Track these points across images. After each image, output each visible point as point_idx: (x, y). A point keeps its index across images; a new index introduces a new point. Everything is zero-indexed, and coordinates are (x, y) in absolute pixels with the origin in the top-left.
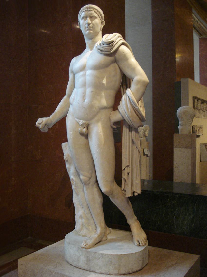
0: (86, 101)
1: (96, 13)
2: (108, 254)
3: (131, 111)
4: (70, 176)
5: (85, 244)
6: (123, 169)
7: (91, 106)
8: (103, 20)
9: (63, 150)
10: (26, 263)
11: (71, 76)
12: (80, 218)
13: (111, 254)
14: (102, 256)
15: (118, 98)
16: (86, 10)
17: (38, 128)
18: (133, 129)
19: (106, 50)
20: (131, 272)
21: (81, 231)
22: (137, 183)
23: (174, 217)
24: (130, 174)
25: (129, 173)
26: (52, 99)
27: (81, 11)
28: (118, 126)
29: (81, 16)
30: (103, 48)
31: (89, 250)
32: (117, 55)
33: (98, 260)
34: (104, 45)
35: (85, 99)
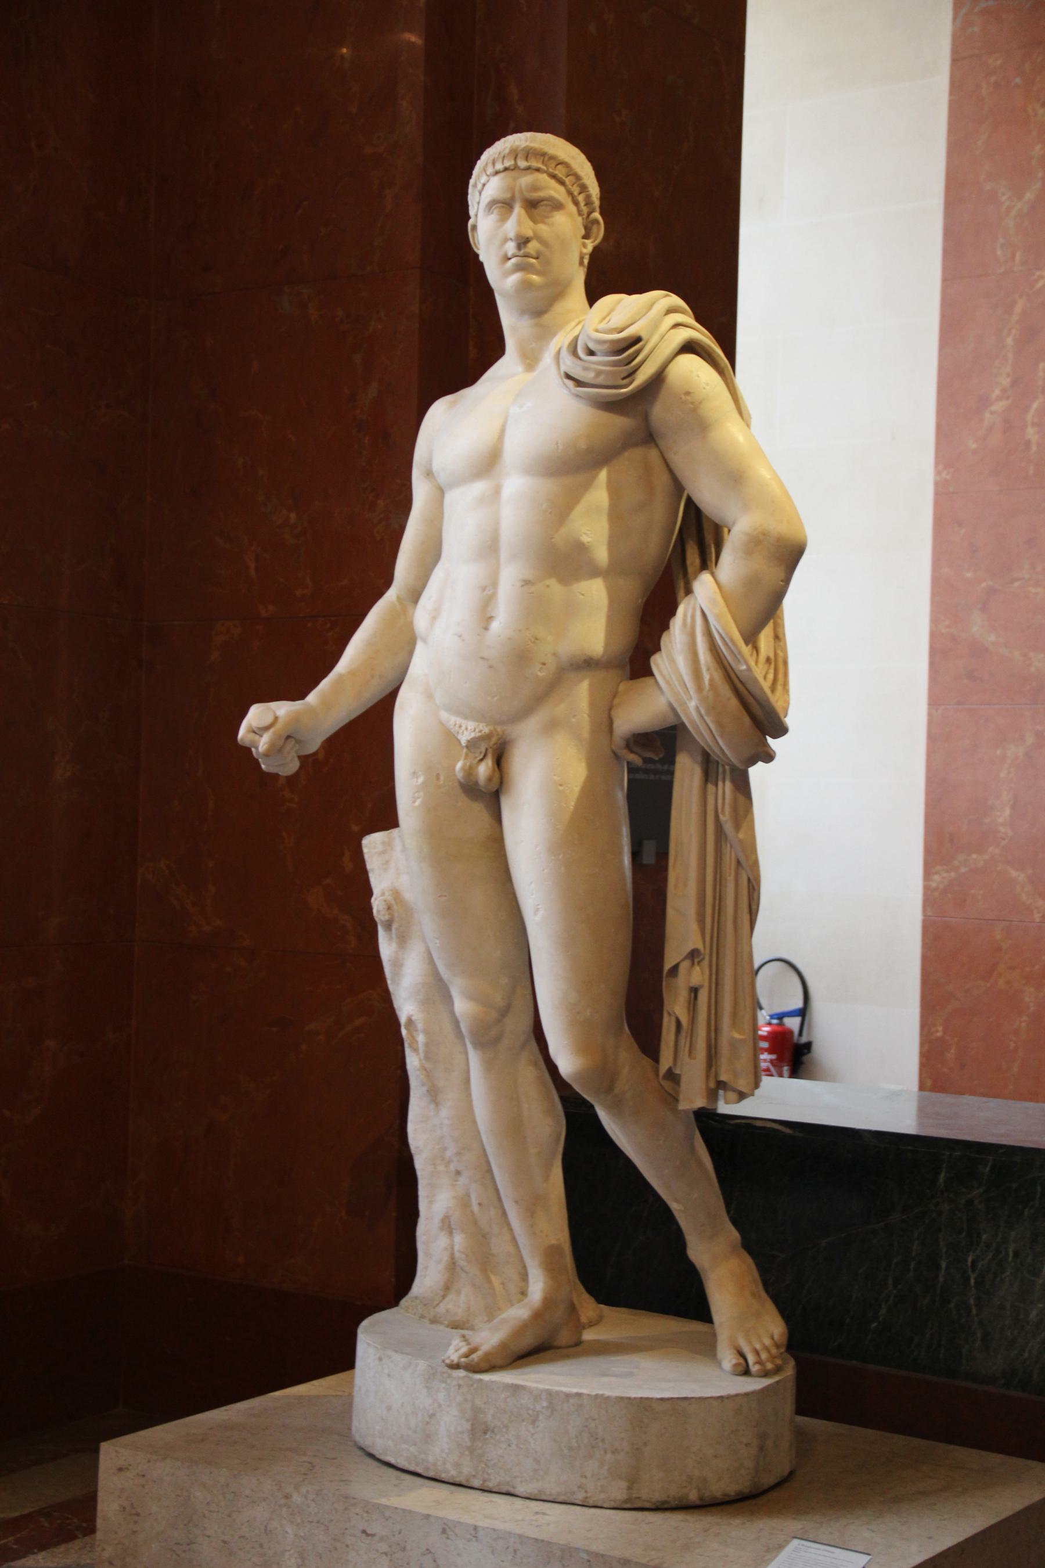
0: (495, 626)
1: (562, 183)
2: (579, 1395)
3: (711, 681)
4: (397, 1004)
5: (464, 1349)
6: (668, 966)
7: (520, 656)
8: (597, 215)
9: (369, 867)
10: (136, 1471)
12: (441, 1229)
14: (551, 1407)
16: (507, 164)
18: (724, 771)
19: (601, 380)
20: (693, 1496)
21: (444, 1297)
22: (733, 1044)
23: (972, 1282)
24: (703, 996)
25: (702, 986)
27: (485, 170)
28: (649, 755)
29: (483, 193)
30: (585, 369)
31: (486, 1377)
32: (658, 411)
33: (530, 1428)
34: (591, 353)
35: (491, 618)
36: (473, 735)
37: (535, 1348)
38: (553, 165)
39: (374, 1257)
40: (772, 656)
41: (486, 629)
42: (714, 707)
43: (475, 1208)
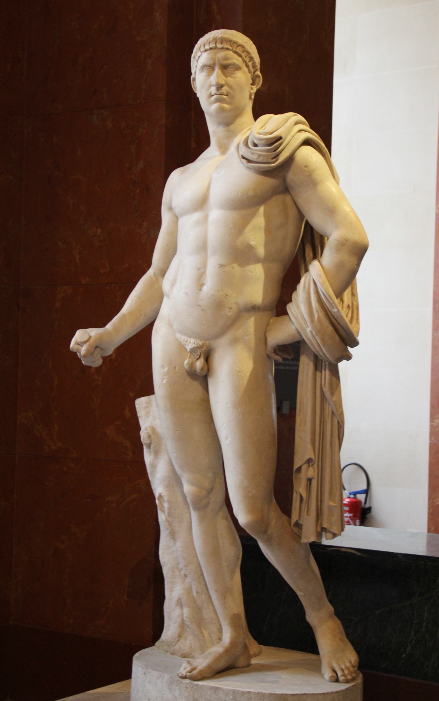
0: (205, 288)
1: (240, 56)
2: (249, 692)
5: (189, 668)
6: (295, 467)
7: (218, 304)
8: (258, 73)
11: (166, 218)
12: (177, 605)
13: (258, 693)
15: (288, 279)
17: (74, 354)
18: (325, 365)
19: (261, 159)
21: (178, 641)
24: (314, 483)
25: (313, 478)
26: (102, 271)
27: (199, 49)
28: (286, 356)
29: (199, 61)
30: (252, 153)
31: (200, 683)
32: (291, 176)
34: (256, 145)
35: (203, 285)
36: (193, 346)
37: (226, 668)
38: (235, 46)
39: (141, 620)
40: (350, 304)
41: (200, 290)
42: (320, 331)
43: (195, 594)
